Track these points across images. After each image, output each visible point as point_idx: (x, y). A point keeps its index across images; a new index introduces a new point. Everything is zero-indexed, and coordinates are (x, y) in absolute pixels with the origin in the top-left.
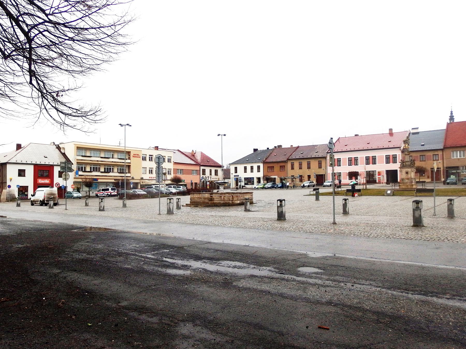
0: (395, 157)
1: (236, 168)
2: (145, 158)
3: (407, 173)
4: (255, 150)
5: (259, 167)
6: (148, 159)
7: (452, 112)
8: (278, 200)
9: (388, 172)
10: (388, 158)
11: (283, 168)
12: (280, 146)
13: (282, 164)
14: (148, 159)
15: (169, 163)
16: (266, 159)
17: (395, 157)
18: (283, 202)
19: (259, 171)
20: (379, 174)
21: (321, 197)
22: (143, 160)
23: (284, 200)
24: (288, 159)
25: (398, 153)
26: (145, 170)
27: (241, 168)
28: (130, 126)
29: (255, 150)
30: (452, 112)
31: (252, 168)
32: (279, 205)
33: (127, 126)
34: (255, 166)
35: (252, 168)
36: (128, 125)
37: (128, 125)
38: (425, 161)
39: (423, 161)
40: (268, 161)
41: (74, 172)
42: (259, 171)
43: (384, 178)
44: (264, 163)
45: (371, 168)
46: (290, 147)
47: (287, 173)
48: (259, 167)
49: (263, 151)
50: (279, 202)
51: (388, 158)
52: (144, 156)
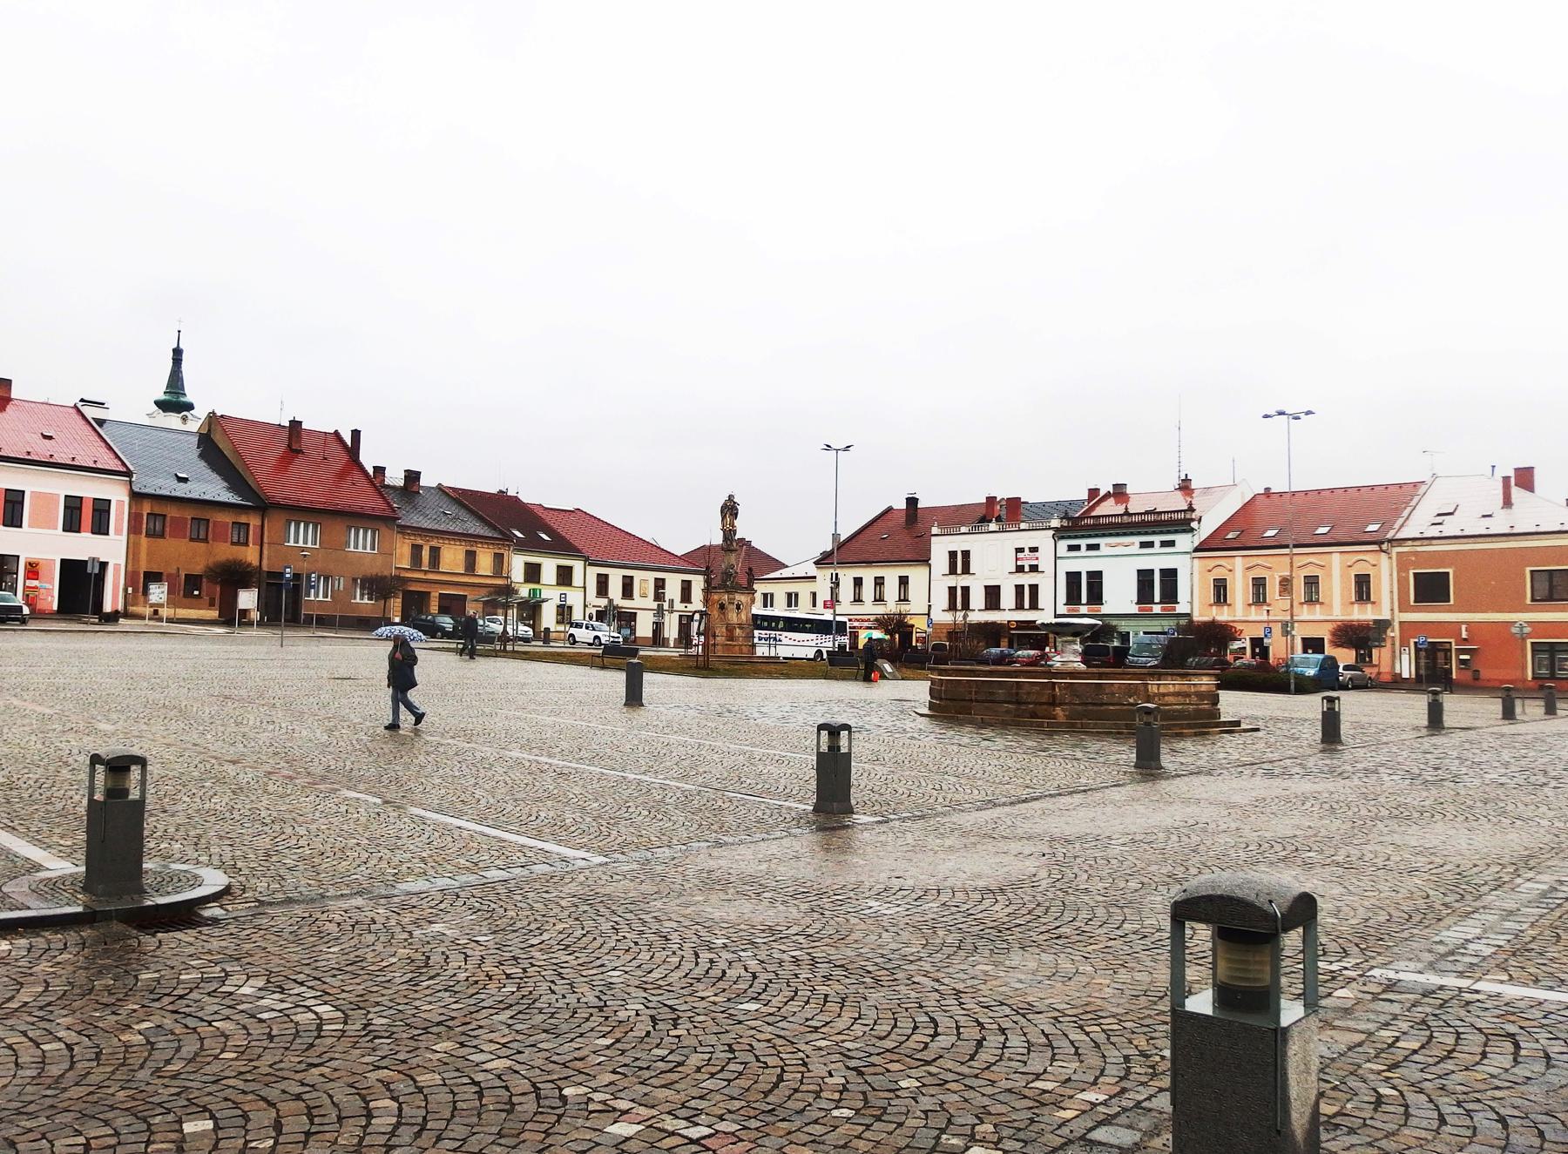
0: (102, 509)
2: (1034, 589)
5: (686, 588)
7: (177, 354)
8: (821, 727)
9: (72, 570)
10: (73, 506)
17: (102, 509)
18: (844, 734)
20: (33, 570)
25: (116, 493)
30: (177, 354)
32: (824, 748)
38: (206, 540)
39: (197, 540)
41: (1320, 656)
43: (50, 592)
45: (84, 546)
47: (132, 552)
48: (686, 588)
50: (824, 733)
51: (73, 506)
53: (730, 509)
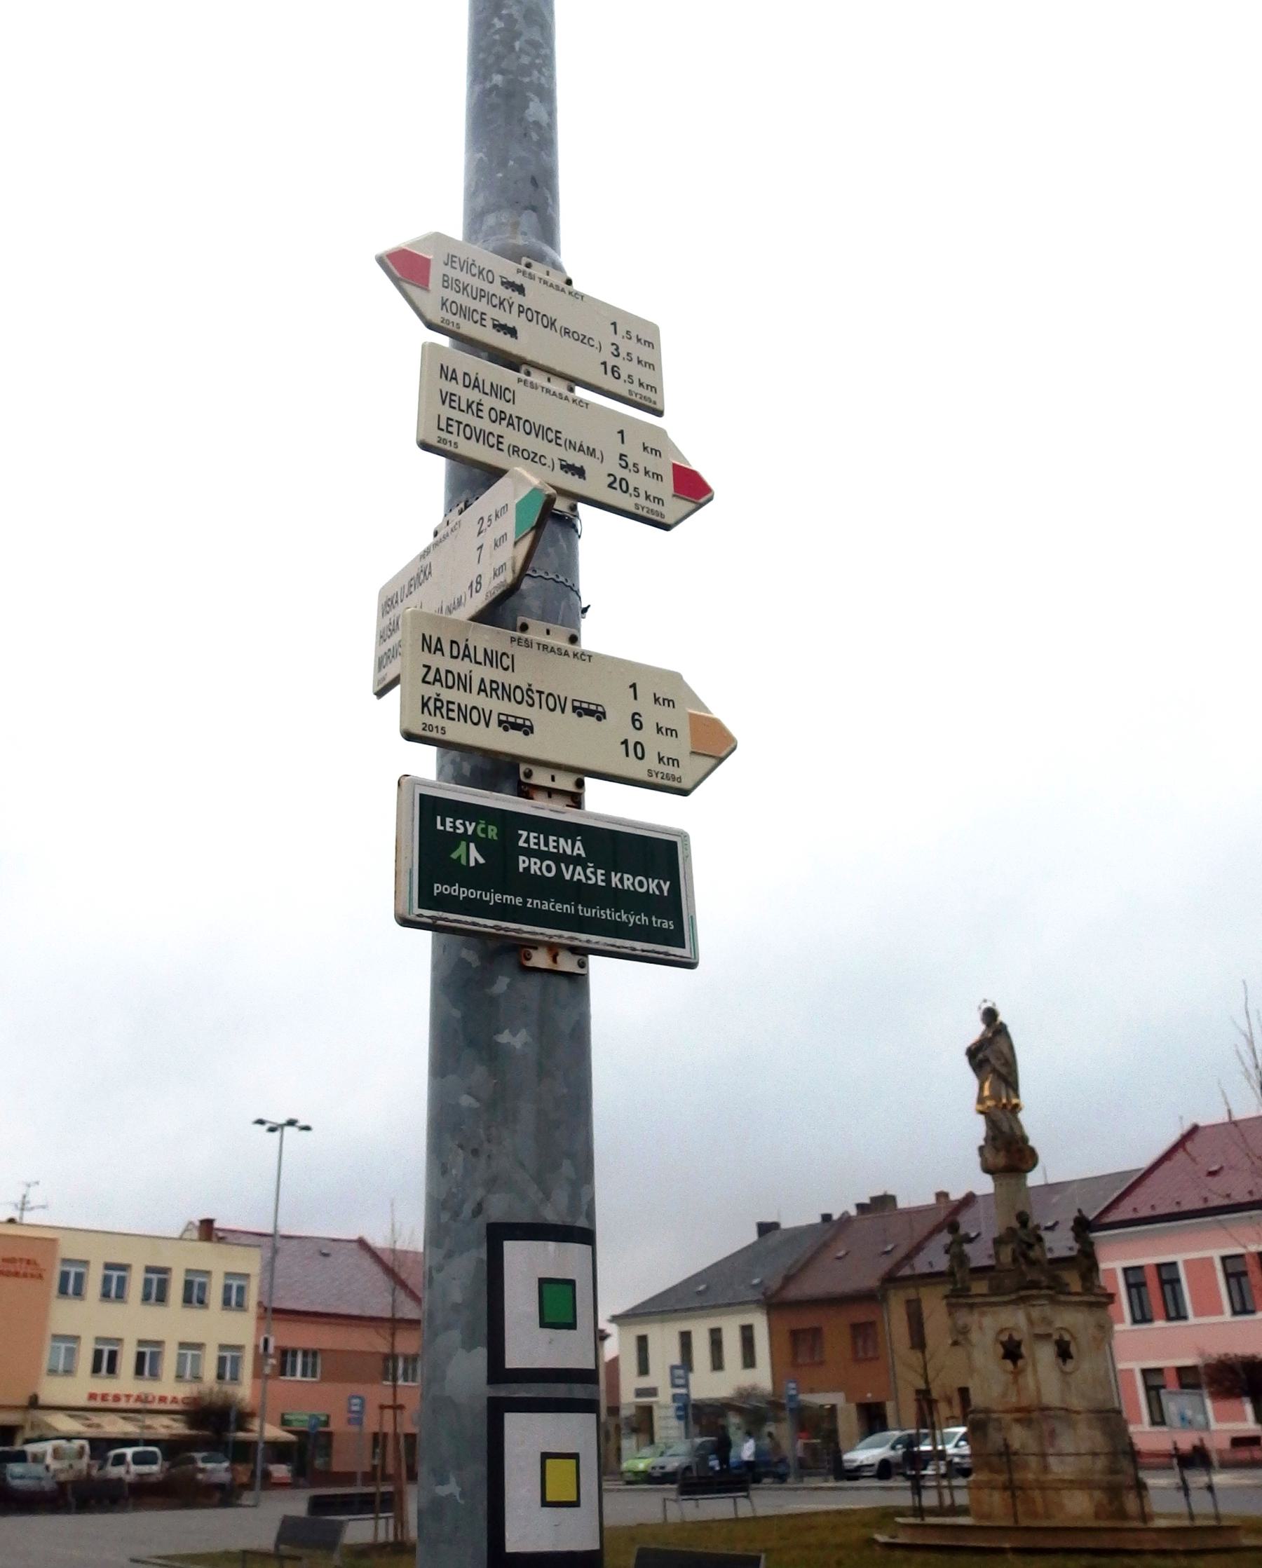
1: (642, 1341)
3: (1012, 1351)
4: (765, 1229)
5: (747, 1334)
6: (93, 1286)
11: (864, 1334)
12: (883, 1203)
13: (860, 1314)
14: (93, 1286)
15: (233, 1316)
16: (788, 1279)
19: (749, 1360)
21: (399, 1402)
22: (63, 1291)
23: (283, 1415)
24: (891, 1279)
26: (71, 1353)
27: (664, 1349)
28: (307, 1128)
29: (765, 1229)
31: (716, 1338)
33: (288, 1129)
34: (731, 1329)
35: (716, 1338)
36: (291, 1123)
37: (291, 1123)
40: (793, 1292)
42: (749, 1360)
44: (774, 1305)
46: (931, 1200)
48: (747, 1334)
49: (799, 1234)
52: (198, 1279)
53: (993, 1056)
